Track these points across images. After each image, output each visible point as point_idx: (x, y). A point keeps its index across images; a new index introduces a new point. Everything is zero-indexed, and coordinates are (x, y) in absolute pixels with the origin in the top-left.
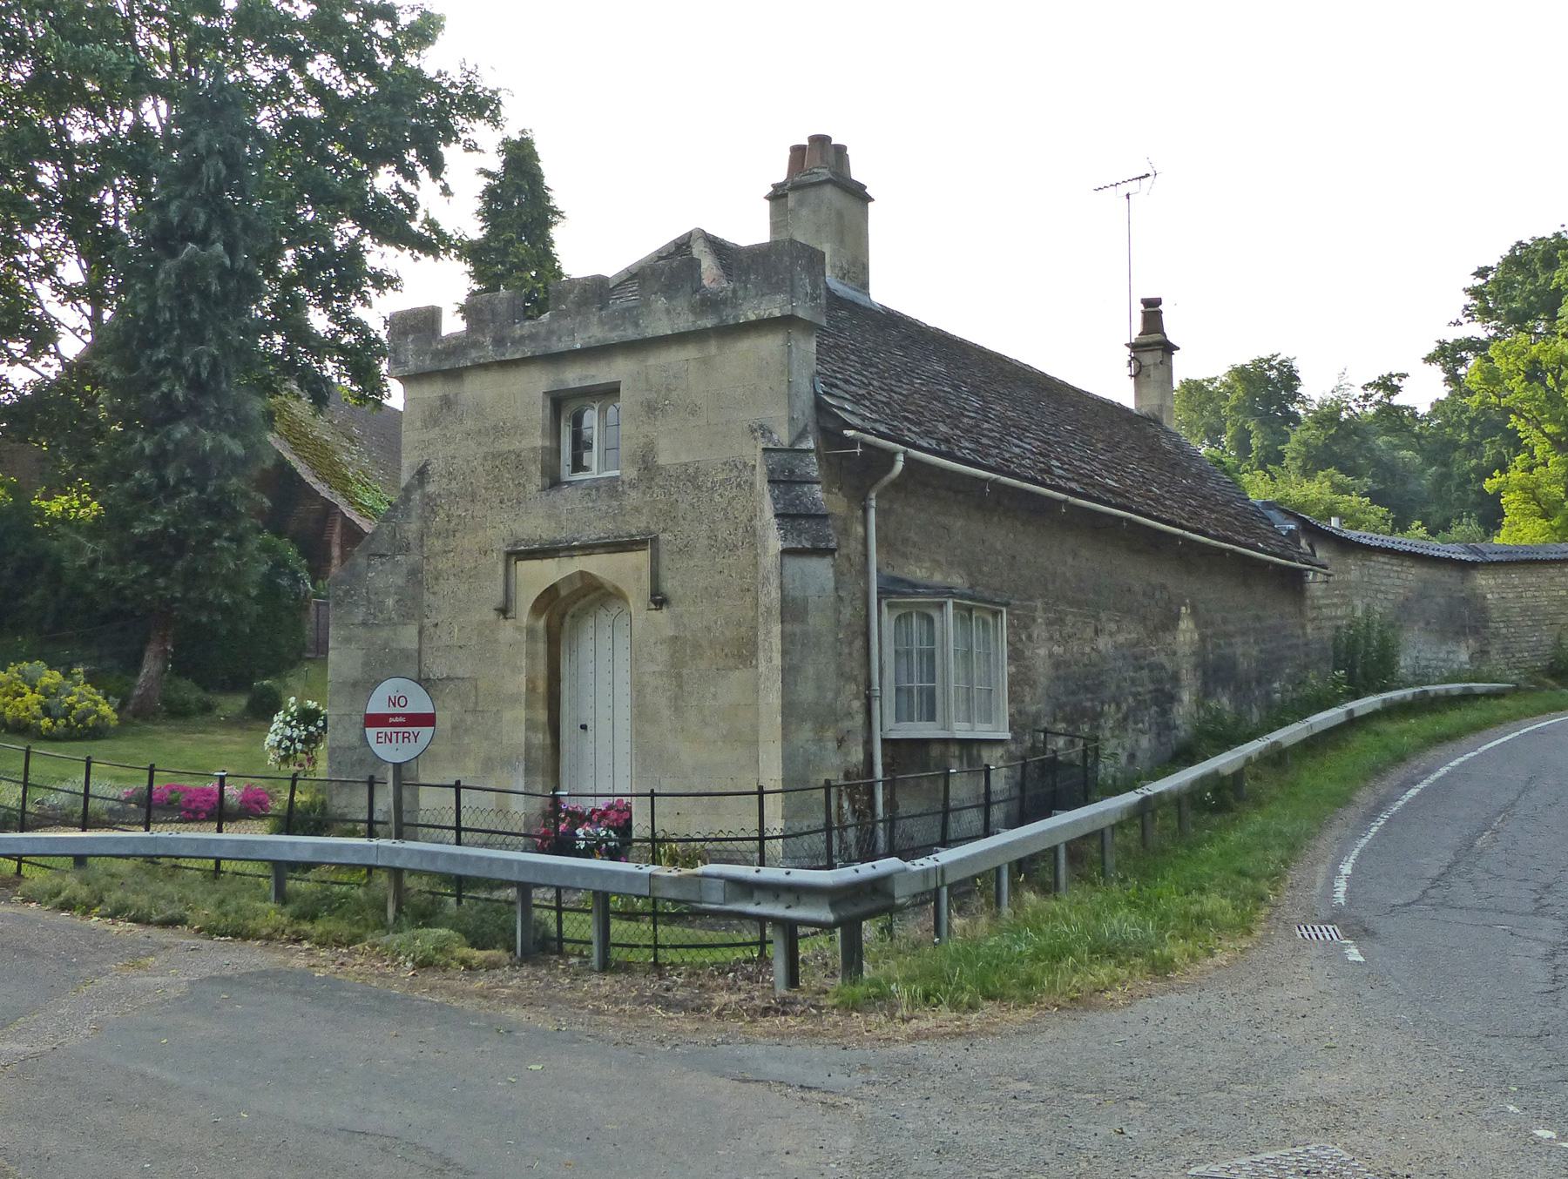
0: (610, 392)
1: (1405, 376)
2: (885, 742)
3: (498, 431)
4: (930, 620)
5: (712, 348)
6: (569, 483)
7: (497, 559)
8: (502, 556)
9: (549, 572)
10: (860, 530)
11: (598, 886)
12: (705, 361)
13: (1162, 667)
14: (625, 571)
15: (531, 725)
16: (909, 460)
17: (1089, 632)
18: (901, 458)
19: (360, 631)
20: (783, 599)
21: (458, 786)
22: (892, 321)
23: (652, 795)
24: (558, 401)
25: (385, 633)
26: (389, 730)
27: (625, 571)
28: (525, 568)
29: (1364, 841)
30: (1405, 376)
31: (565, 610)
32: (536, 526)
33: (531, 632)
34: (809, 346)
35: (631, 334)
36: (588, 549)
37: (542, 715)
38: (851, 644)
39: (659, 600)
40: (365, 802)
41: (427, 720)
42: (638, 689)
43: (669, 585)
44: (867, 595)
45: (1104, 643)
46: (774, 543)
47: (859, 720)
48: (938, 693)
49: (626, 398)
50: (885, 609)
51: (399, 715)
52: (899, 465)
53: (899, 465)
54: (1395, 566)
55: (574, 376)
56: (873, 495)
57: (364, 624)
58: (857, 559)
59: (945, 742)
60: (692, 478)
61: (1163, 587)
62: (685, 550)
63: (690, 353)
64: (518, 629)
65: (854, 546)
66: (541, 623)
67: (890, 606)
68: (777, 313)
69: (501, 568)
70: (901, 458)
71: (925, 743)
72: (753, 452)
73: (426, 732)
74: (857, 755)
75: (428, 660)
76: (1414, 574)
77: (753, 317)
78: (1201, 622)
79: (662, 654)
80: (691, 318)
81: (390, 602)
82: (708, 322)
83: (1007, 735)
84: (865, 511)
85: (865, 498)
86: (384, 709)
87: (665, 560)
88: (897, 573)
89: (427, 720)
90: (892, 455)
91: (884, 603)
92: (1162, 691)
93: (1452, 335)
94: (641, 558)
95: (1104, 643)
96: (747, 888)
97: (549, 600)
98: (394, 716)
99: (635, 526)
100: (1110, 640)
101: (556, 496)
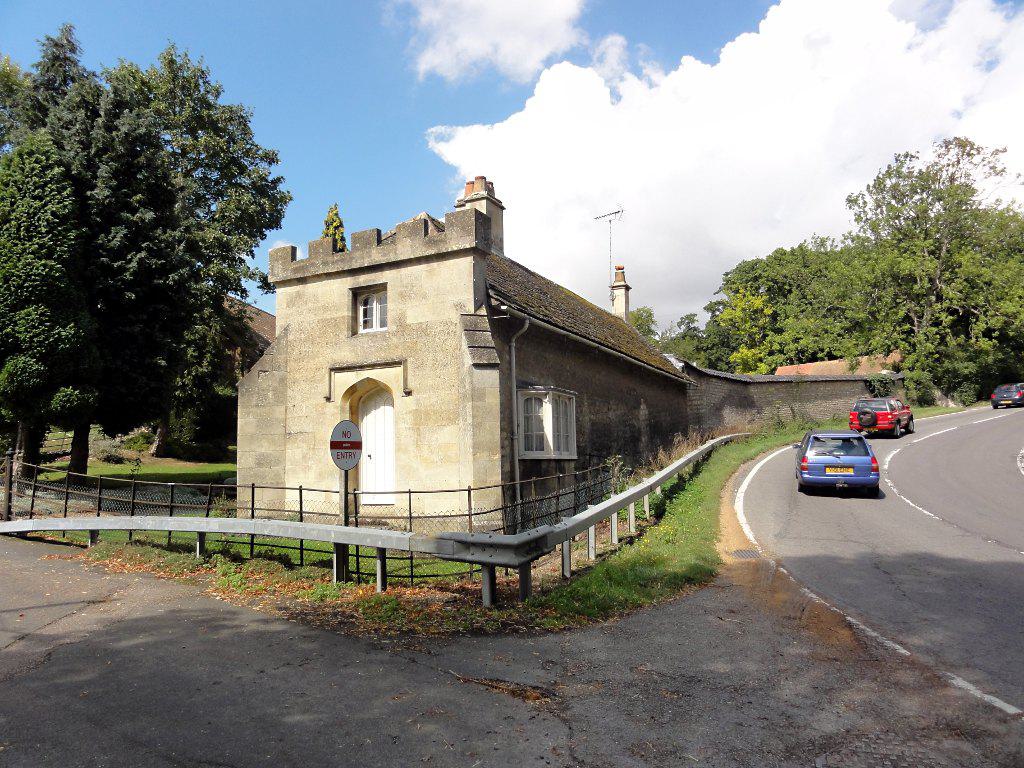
0: (383, 287)
3: (325, 308)
5: (435, 265)
6: (362, 335)
7: (325, 372)
8: (328, 371)
10: (508, 357)
11: (380, 545)
12: (429, 272)
13: (635, 426)
16: (531, 324)
17: (606, 409)
18: (528, 322)
19: (255, 409)
20: (473, 389)
21: (301, 489)
23: (410, 492)
24: (356, 293)
26: (343, 451)
27: (388, 376)
28: (338, 377)
31: (365, 397)
32: (346, 356)
35: (392, 258)
36: (373, 366)
42: (398, 436)
43: (411, 385)
44: (511, 389)
45: (611, 415)
46: (468, 361)
49: (390, 292)
50: (519, 396)
51: (348, 442)
52: (527, 325)
53: (527, 325)
54: (719, 383)
55: (363, 280)
57: (257, 406)
59: (549, 460)
60: (424, 330)
61: (635, 390)
62: (420, 366)
63: (422, 268)
64: (337, 407)
68: (468, 246)
69: (327, 376)
70: (528, 322)
72: (455, 317)
75: (290, 423)
76: (727, 387)
77: (455, 249)
78: (649, 406)
79: (409, 418)
81: (270, 394)
82: (432, 251)
83: (575, 457)
84: (510, 347)
85: (510, 341)
87: (410, 372)
88: (524, 379)
90: (524, 320)
91: (519, 393)
92: (634, 436)
93: (715, 299)
94: (399, 370)
95: (611, 415)
98: (345, 442)
99: (395, 356)
100: (613, 414)
101: (354, 340)
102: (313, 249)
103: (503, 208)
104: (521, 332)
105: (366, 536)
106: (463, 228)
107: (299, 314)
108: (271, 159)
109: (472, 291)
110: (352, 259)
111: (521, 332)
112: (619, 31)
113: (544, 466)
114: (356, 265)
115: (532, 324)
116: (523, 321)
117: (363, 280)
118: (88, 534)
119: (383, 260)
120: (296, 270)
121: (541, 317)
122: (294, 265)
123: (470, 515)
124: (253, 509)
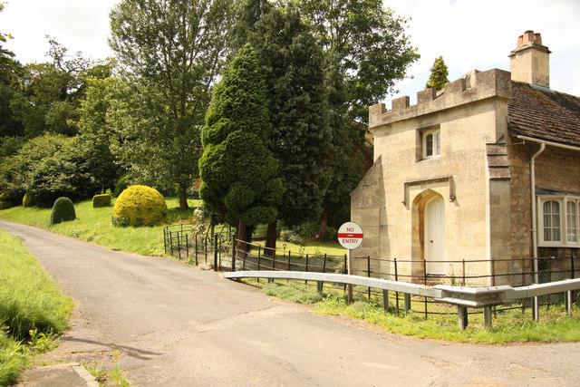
1: (12, 38)
2: (539, 248)
4: (558, 204)
9: (414, 192)
10: (528, 172)
14: (444, 190)
15: (413, 241)
22: (558, 97)
23: (464, 262)
25: (368, 211)
29: (508, 287)
30: (12, 38)
32: (417, 176)
33: (413, 211)
34: (505, 107)
35: (442, 107)
37: (418, 237)
38: (524, 213)
39: (453, 198)
40: (570, 265)
41: (360, 236)
46: (488, 177)
47: (528, 239)
48: (561, 232)
55: (425, 123)
56: (533, 159)
58: (528, 182)
59: (565, 249)
60: (463, 155)
65: (526, 178)
66: (417, 207)
67: (542, 199)
71: (556, 249)
73: (360, 240)
74: (527, 252)
80: (462, 99)
82: (467, 101)
84: (530, 164)
86: (345, 232)
89: (360, 236)
96: (449, 294)
97: (419, 198)
99: (444, 174)
102: (420, 95)
103: (549, 52)
104: (538, 153)
105: (374, 282)
106: (487, 84)
107: (393, 150)
108: (396, 26)
109: (495, 126)
110: (417, 109)
111: (538, 153)
112: (205, 201)
113: (560, 252)
114: (420, 114)
115: (547, 146)
116: (538, 146)
117: (425, 123)
118: (316, 283)
119: (436, 109)
120: (385, 119)
121: (560, 139)
122: (384, 116)
123: (464, 278)
124: (396, 275)
